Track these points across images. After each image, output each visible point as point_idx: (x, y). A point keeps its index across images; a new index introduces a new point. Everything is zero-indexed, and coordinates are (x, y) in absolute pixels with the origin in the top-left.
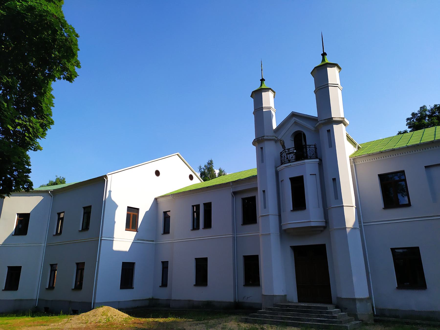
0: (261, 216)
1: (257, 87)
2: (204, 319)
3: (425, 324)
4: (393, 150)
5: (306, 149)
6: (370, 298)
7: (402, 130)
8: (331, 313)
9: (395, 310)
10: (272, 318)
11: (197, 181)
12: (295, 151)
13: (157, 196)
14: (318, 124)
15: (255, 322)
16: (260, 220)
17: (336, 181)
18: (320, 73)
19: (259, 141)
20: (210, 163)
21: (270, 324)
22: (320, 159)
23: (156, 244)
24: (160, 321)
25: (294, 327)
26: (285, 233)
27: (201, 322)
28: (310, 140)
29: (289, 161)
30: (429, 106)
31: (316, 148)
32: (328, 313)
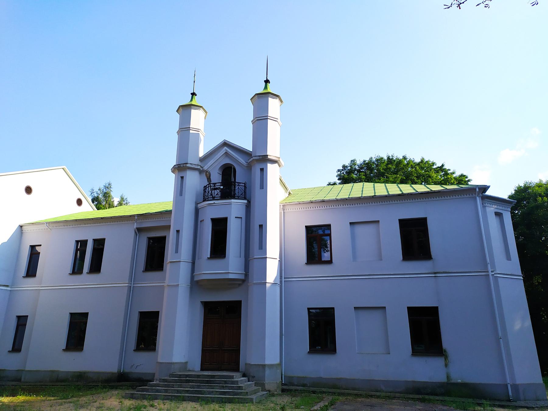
0: (171, 262)
1: (187, 102)
2: (72, 397)
3: (330, 393)
4: (323, 201)
5: (235, 187)
6: (280, 364)
7: (332, 181)
8: (237, 382)
9: (303, 377)
10: (166, 391)
11: (88, 210)
12: (222, 187)
13: (21, 223)
14: (252, 159)
15: (144, 397)
16: (168, 267)
17: (262, 228)
18: (261, 98)
19: (180, 168)
20: (108, 187)
21: (164, 399)
22: (248, 201)
23: (11, 290)
24: (3, 401)
25: (192, 401)
26: (196, 285)
27: (68, 400)
28: (240, 177)
29: (214, 198)
30: (359, 161)
31: (245, 187)
32: (233, 383)
